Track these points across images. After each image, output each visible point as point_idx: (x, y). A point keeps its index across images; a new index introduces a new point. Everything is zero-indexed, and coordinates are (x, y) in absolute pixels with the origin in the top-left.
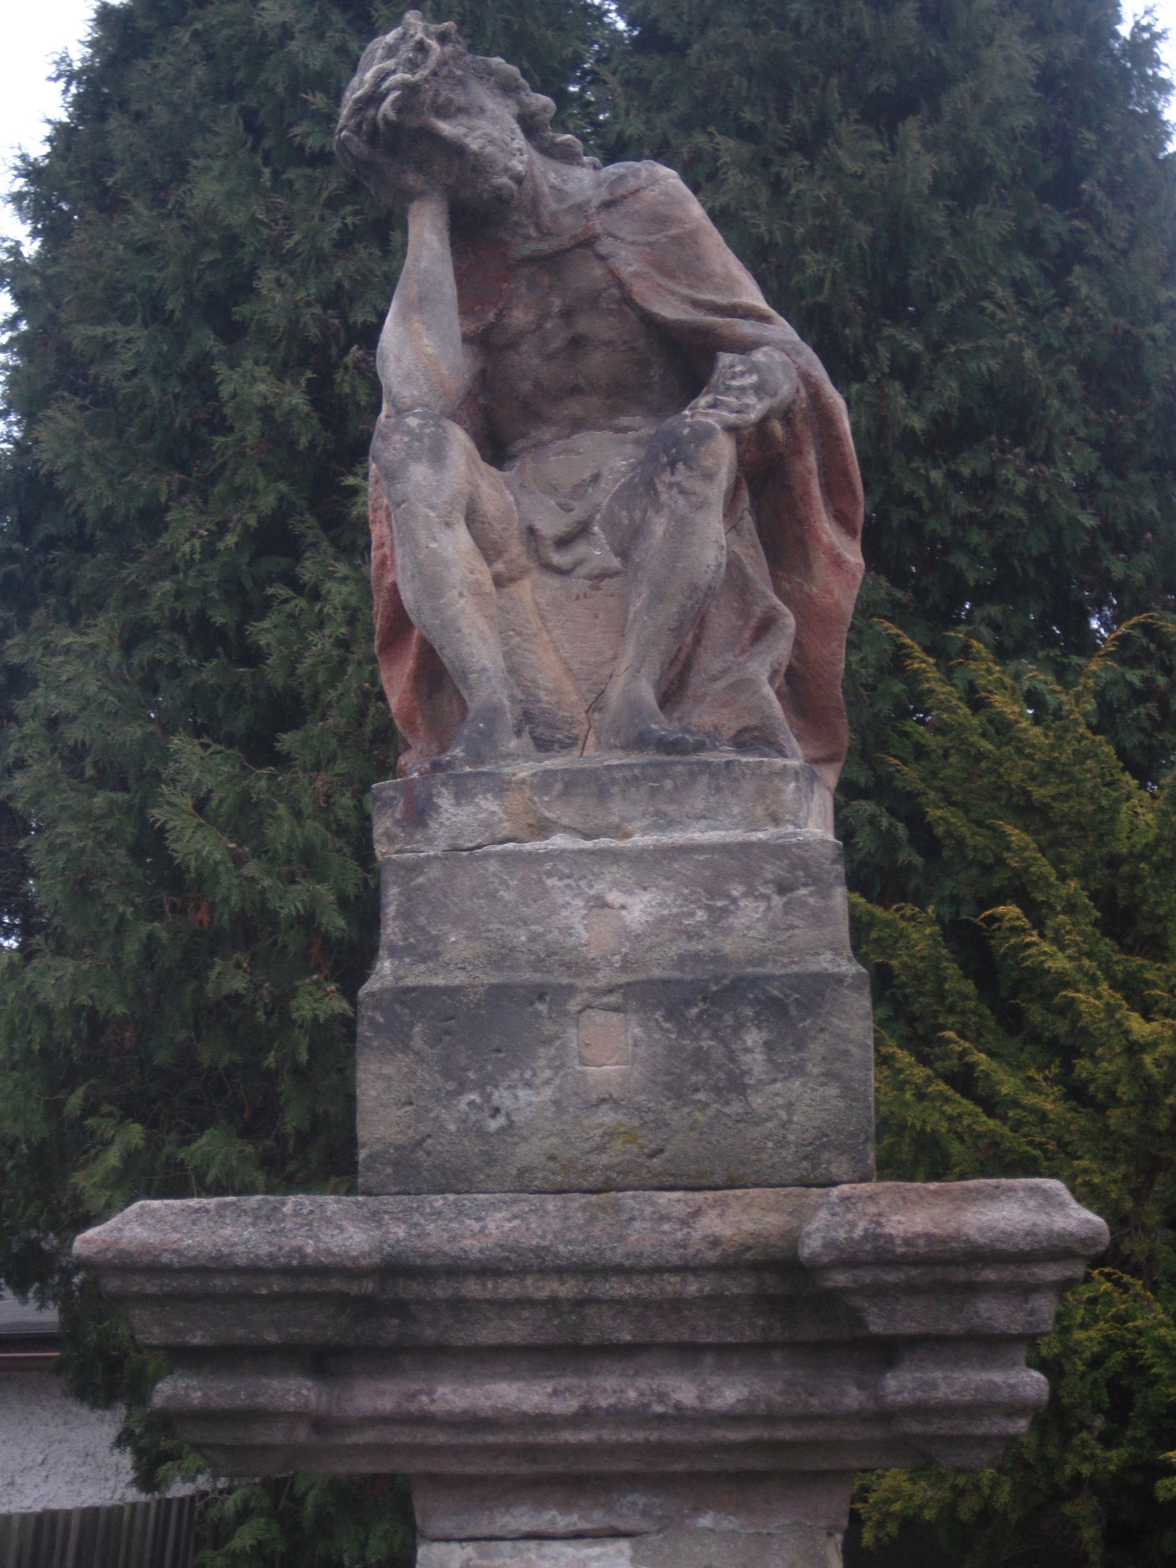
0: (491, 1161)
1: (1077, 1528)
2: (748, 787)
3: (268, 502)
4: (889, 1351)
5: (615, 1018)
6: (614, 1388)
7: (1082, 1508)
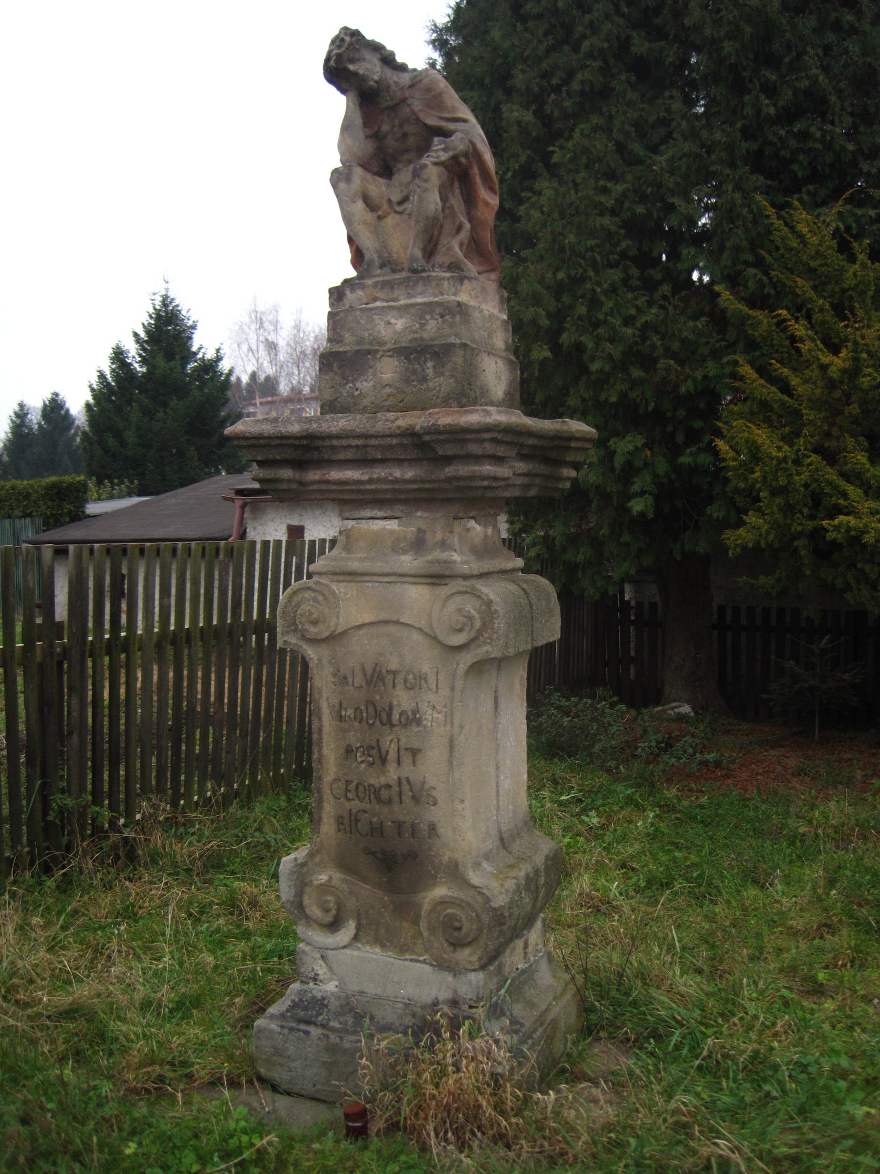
0: (356, 405)
2: (434, 284)
3: (523, 158)
4: (448, 460)
5: (391, 359)
6: (379, 472)
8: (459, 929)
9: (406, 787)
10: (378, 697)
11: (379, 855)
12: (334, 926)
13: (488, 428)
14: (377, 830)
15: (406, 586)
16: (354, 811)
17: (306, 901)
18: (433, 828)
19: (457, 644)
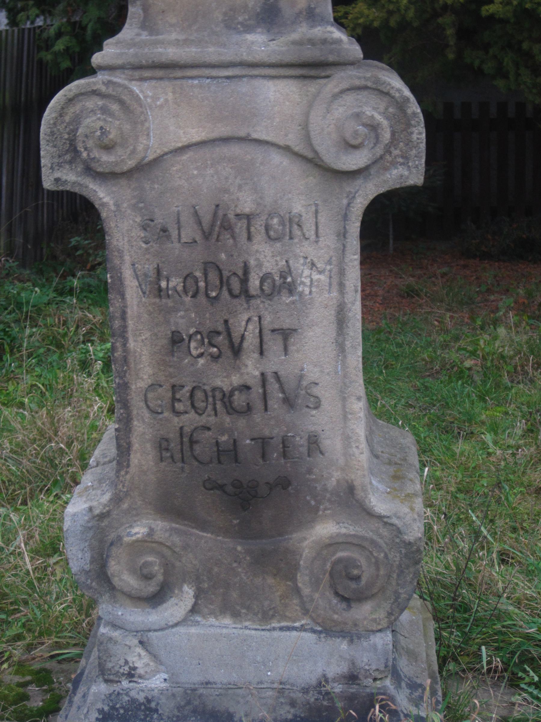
1: (444, 29)
7: (447, 20)
8: (358, 578)
9: (273, 386)
10: (223, 256)
11: (230, 489)
12: (156, 599)
14: (230, 453)
16: (187, 430)
17: (113, 567)
18: (314, 443)
19: (354, 168)
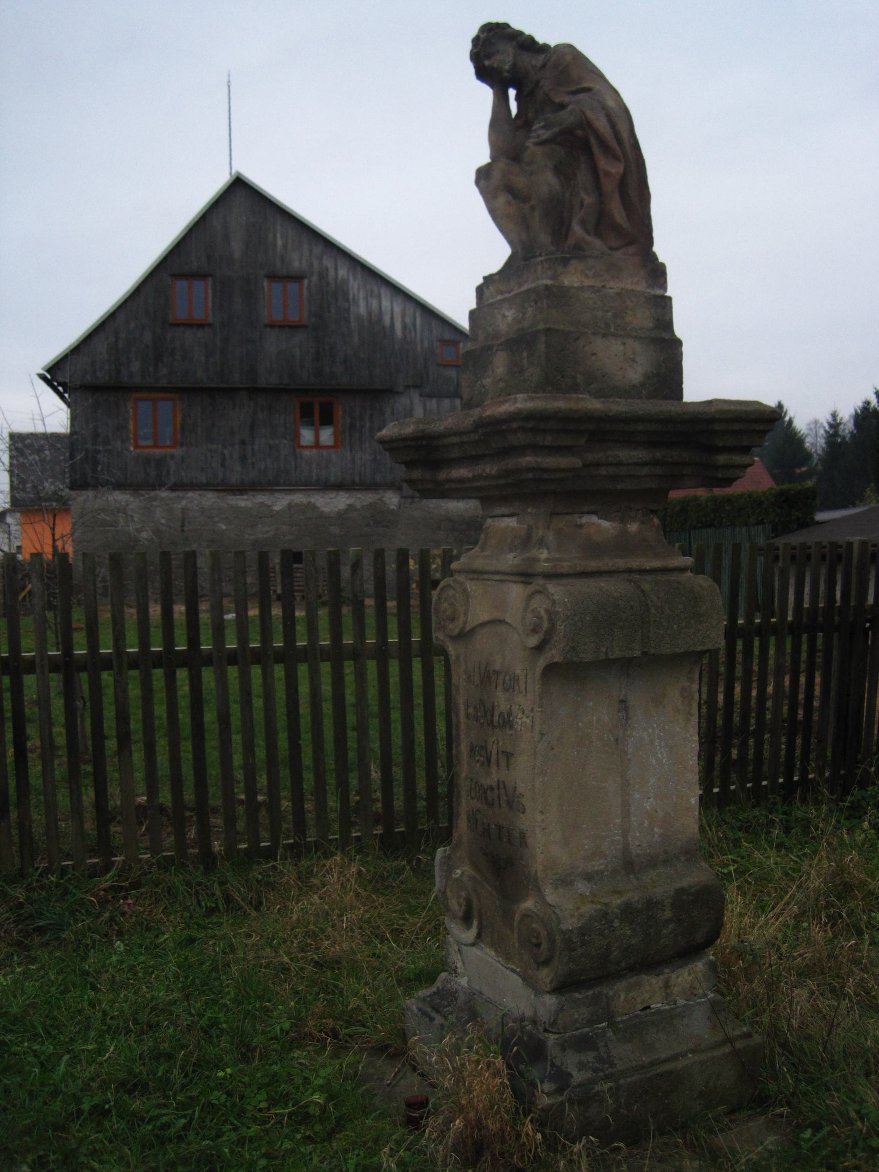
13: (512, 417)
15: (512, 585)
18: (523, 836)
